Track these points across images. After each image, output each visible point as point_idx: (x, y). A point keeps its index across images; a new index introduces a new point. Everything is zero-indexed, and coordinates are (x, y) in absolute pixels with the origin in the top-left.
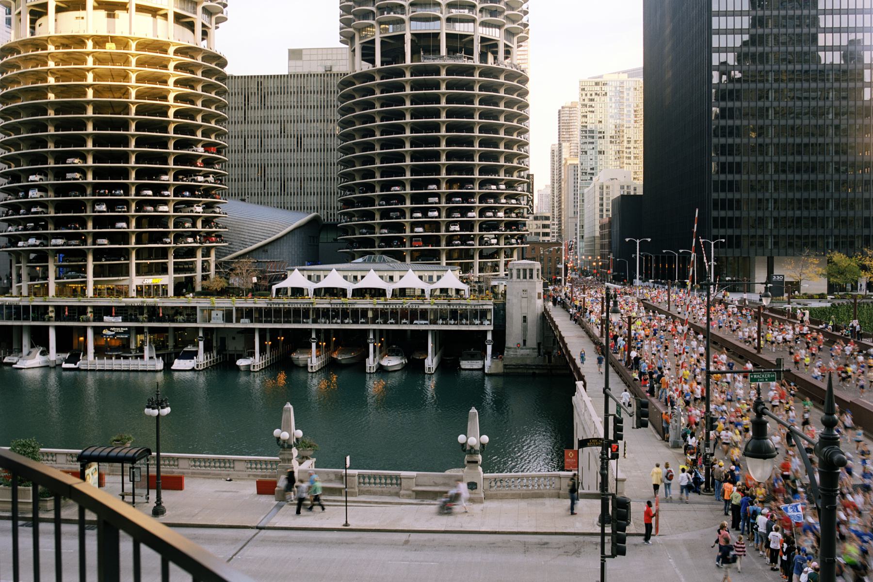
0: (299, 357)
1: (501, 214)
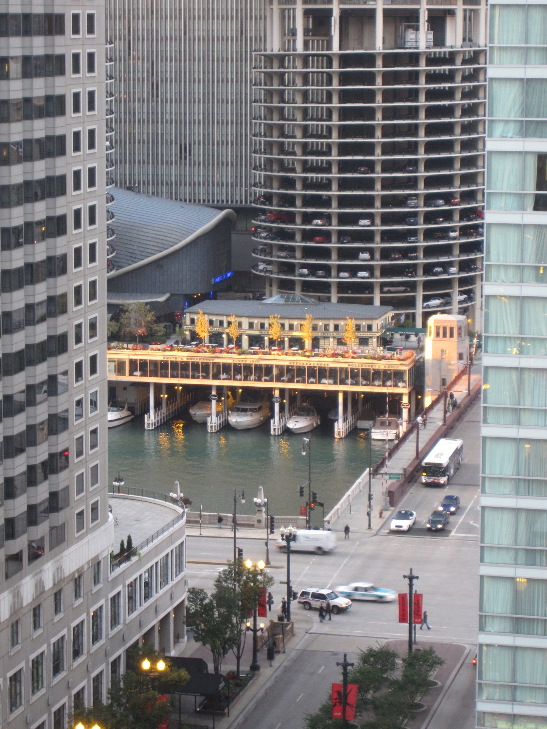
0: (196, 413)
1: (454, 270)
